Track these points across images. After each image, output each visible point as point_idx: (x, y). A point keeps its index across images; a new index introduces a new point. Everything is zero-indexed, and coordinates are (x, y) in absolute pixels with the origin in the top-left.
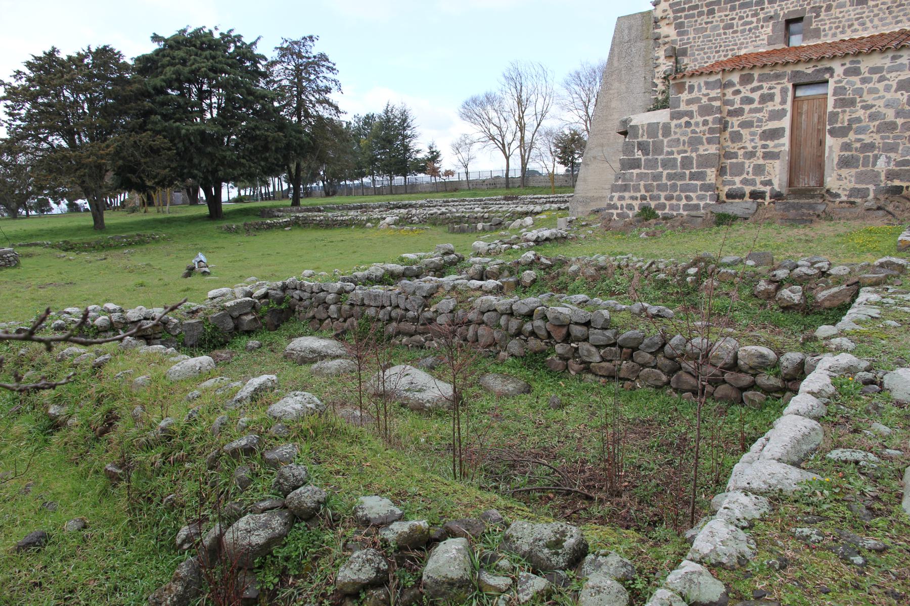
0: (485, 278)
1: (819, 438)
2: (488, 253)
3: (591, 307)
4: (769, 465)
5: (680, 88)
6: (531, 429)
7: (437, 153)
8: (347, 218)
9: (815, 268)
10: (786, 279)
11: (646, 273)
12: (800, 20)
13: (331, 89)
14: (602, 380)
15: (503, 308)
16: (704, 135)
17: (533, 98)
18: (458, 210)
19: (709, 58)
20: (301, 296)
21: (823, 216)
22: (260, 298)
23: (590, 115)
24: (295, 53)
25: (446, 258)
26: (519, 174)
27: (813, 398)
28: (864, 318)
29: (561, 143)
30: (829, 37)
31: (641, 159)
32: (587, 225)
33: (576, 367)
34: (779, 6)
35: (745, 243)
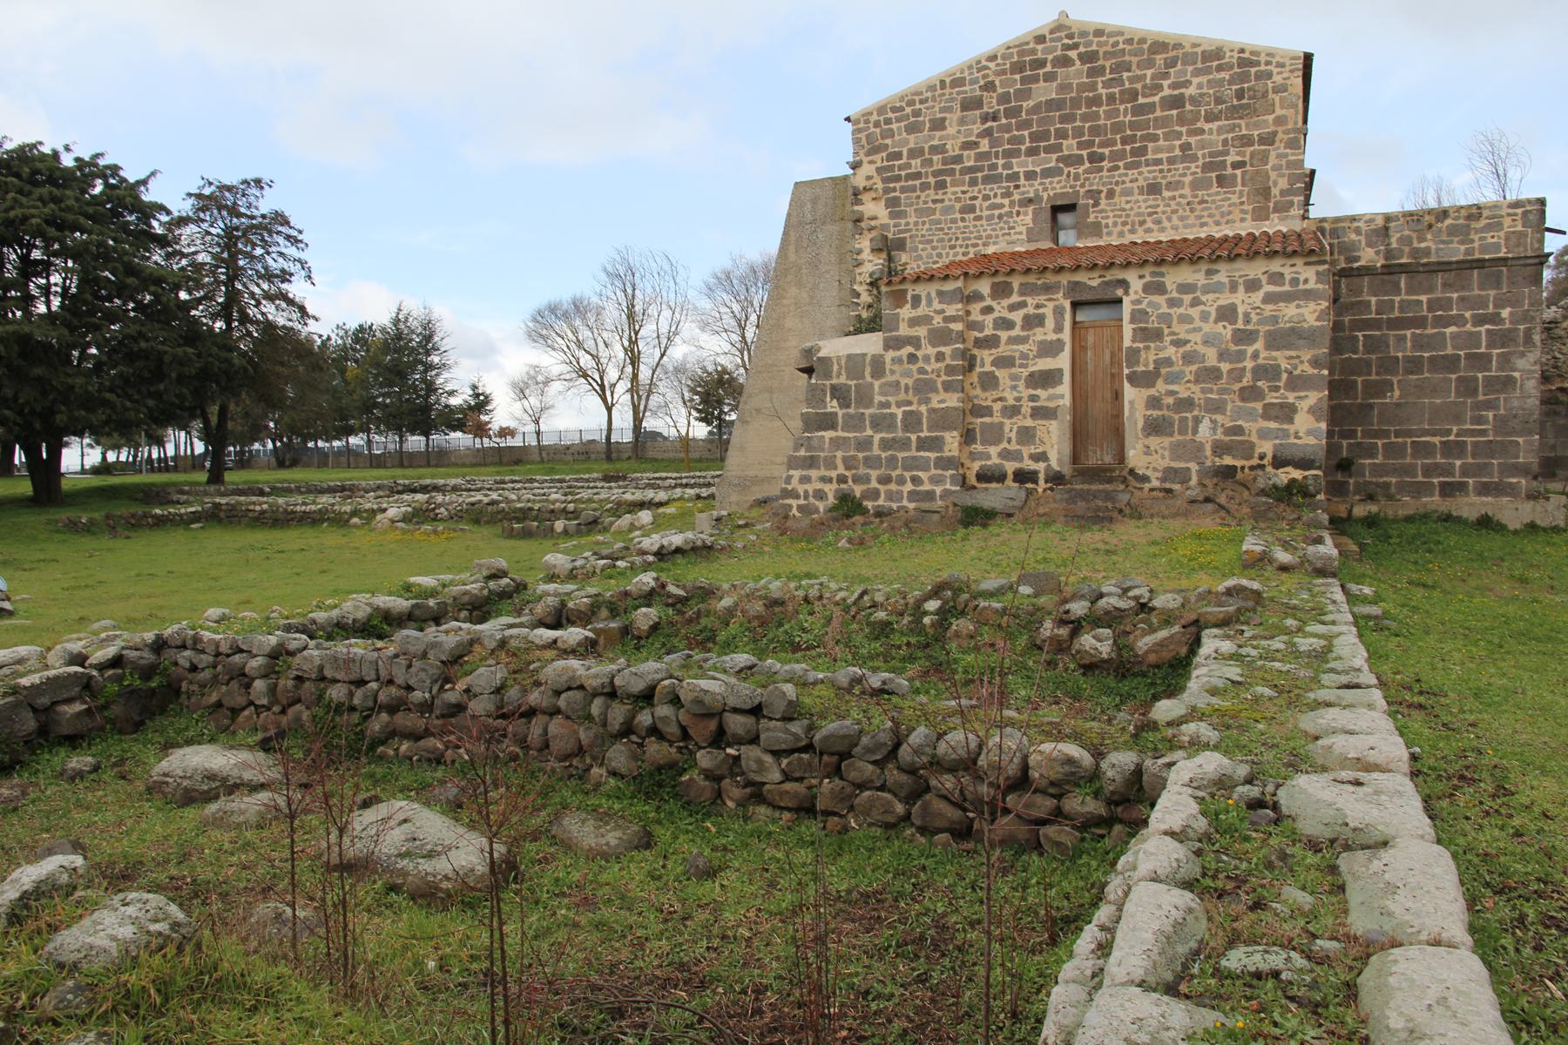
0: (564, 622)
1: (1200, 928)
2: (572, 576)
3: (762, 679)
4: (1130, 1000)
5: (899, 298)
6: (654, 924)
7: (486, 397)
8: (313, 507)
9: (1129, 598)
10: (1085, 618)
11: (853, 610)
12: (1070, 208)
13: (291, 275)
14: (787, 815)
15: (596, 683)
16: (939, 376)
17: (653, 310)
18: (519, 495)
19: (939, 255)
20: (195, 661)
21: (1127, 511)
22: (102, 667)
23: (749, 341)
24: (226, 207)
25: (492, 584)
26: (628, 437)
27: (1177, 844)
28: (1220, 684)
29: (700, 386)
30: (1114, 236)
31: (836, 414)
32: (746, 525)
33: (737, 792)
34: (1041, 184)
35: (1012, 556)
